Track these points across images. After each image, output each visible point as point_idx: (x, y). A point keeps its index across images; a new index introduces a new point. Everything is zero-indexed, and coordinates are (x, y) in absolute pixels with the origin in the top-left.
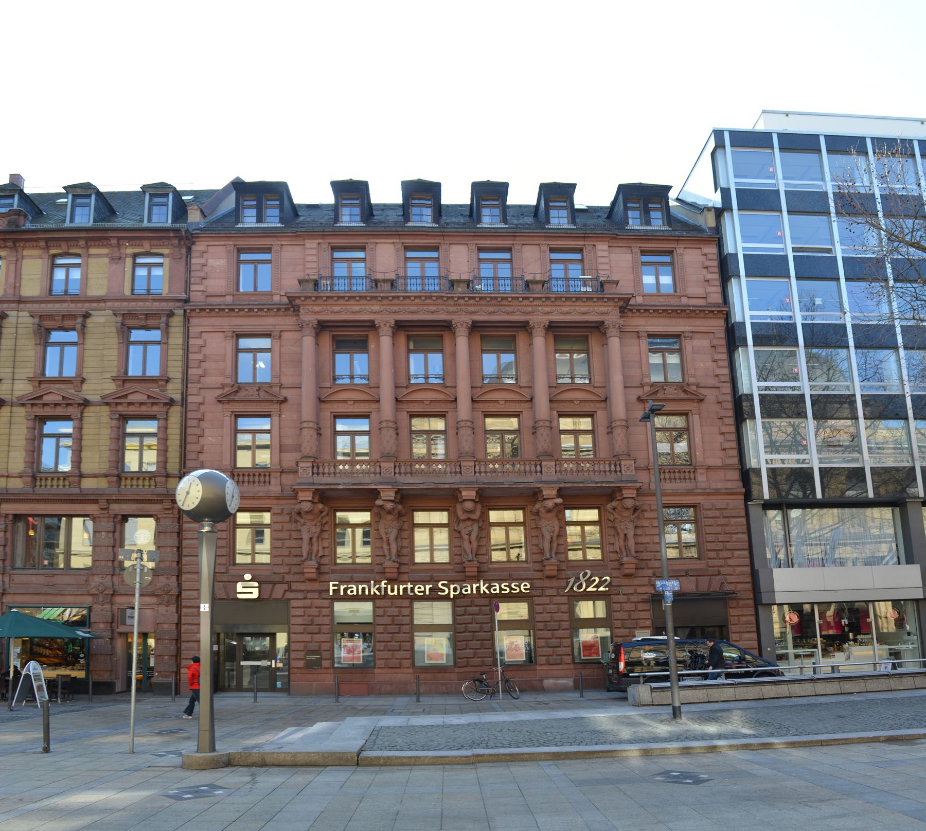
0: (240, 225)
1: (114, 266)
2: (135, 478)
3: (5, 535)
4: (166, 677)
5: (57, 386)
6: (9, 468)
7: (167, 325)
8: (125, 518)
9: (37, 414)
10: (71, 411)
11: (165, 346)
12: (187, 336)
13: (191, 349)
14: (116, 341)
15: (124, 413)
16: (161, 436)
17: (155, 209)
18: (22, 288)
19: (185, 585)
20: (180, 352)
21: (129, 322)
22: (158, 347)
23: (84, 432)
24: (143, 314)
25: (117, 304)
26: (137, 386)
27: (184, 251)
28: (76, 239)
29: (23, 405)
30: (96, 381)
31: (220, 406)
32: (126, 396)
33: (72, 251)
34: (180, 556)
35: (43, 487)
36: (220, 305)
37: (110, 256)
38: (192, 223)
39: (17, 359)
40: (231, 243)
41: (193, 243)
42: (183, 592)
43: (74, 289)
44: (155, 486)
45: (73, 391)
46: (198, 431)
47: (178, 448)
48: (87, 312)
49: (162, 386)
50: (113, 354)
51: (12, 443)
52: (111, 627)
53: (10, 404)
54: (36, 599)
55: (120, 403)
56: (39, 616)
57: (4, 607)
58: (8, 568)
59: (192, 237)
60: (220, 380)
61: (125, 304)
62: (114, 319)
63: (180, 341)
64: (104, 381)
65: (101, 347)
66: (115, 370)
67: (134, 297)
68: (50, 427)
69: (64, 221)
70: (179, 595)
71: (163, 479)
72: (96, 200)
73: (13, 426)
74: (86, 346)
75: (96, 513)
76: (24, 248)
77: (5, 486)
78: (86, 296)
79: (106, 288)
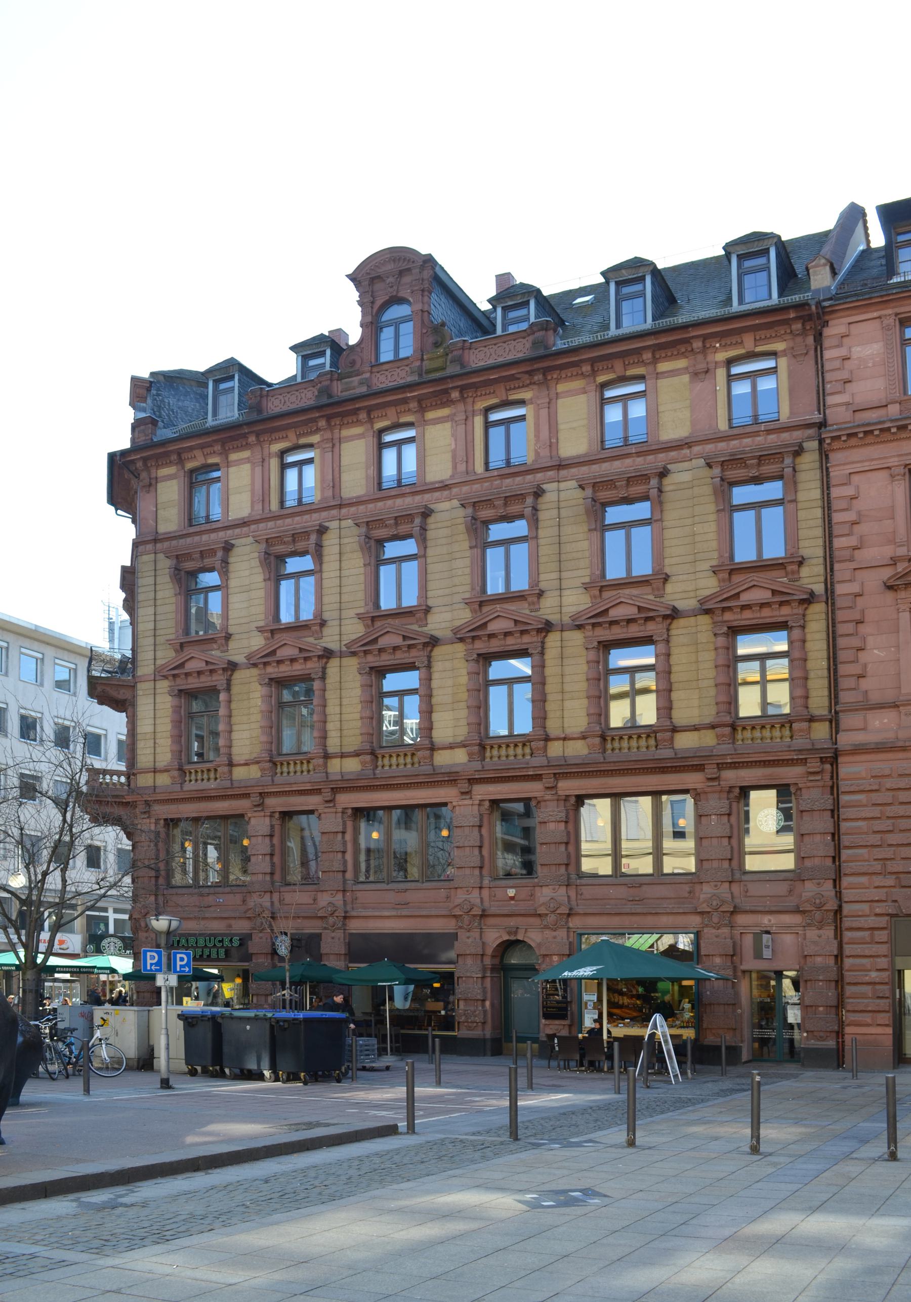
0: (895, 280)
1: (699, 386)
2: (617, 738)
3: (566, 827)
4: (821, 1039)
5: (627, 591)
6: (566, 725)
7: (535, 509)
8: (580, 800)
9: (602, 639)
10: (652, 628)
11: (792, 505)
12: (826, 485)
13: (836, 505)
14: (712, 508)
15: (735, 624)
16: (797, 654)
17: (748, 280)
18: (561, 445)
19: (847, 894)
20: (818, 513)
21: (604, 495)
22: (780, 510)
23: (674, 659)
24: (753, 458)
25: (709, 447)
26: (755, 578)
27: (810, 340)
28: (638, 351)
29: (580, 627)
30: (685, 577)
31: (890, 596)
32: (737, 596)
33: (514, 397)
34: (838, 848)
35: (617, 751)
36: (883, 422)
37: (691, 370)
38: (817, 291)
39: (563, 557)
40: (889, 311)
41: (826, 324)
42: (844, 905)
43: (637, 434)
44: (791, 737)
45: (651, 597)
46: (855, 642)
47: (825, 673)
48: (320, 525)
49: (793, 572)
50: (709, 530)
51: (567, 688)
52: (732, 963)
53: (338, 654)
54: (616, 921)
55: (729, 609)
56: (629, 943)
57: (572, 934)
58: (573, 876)
59: (824, 313)
60: (888, 551)
61: (722, 445)
62: (707, 472)
63: (816, 494)
64: (699, 575)
65: (689, 521)
66: (715, 555)
67: (735, 431)
68: (497, 669)
69: (606, 327)
70: (838, 911)
71: (805, 725)
72: (653, 283)
73: (566, 662)
74: (665, 523)
75: (698, 786)
76: (558, 380)
77: (561, 754)
78: (426, 484)
79: (688, 423)
